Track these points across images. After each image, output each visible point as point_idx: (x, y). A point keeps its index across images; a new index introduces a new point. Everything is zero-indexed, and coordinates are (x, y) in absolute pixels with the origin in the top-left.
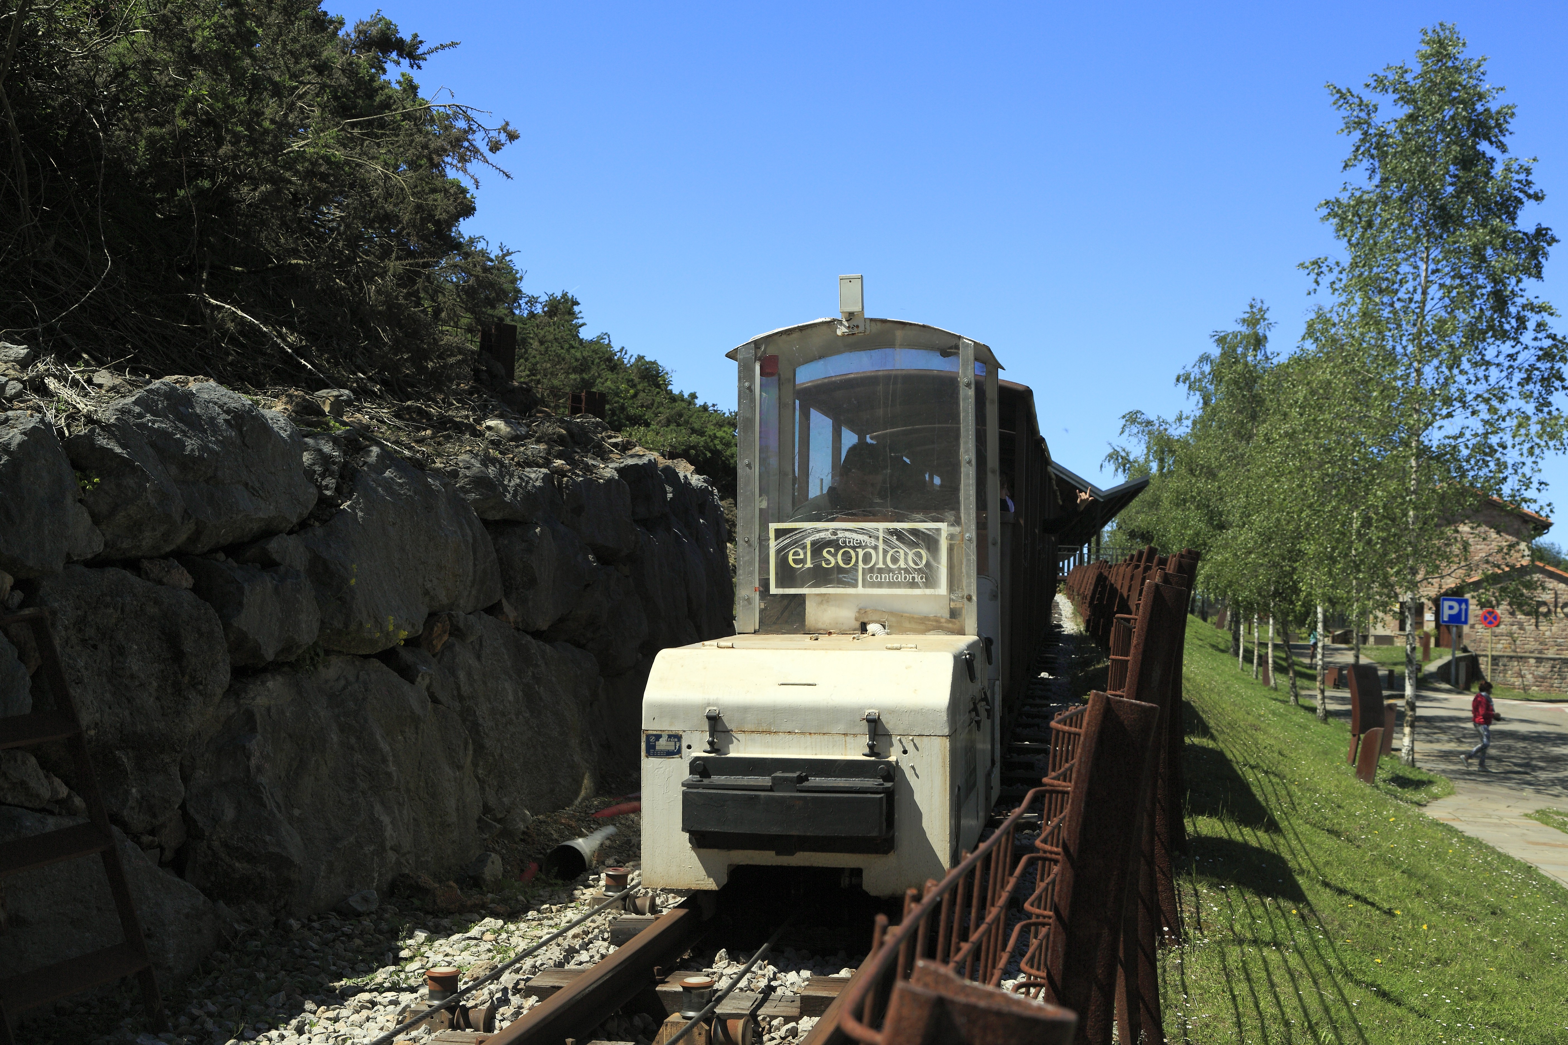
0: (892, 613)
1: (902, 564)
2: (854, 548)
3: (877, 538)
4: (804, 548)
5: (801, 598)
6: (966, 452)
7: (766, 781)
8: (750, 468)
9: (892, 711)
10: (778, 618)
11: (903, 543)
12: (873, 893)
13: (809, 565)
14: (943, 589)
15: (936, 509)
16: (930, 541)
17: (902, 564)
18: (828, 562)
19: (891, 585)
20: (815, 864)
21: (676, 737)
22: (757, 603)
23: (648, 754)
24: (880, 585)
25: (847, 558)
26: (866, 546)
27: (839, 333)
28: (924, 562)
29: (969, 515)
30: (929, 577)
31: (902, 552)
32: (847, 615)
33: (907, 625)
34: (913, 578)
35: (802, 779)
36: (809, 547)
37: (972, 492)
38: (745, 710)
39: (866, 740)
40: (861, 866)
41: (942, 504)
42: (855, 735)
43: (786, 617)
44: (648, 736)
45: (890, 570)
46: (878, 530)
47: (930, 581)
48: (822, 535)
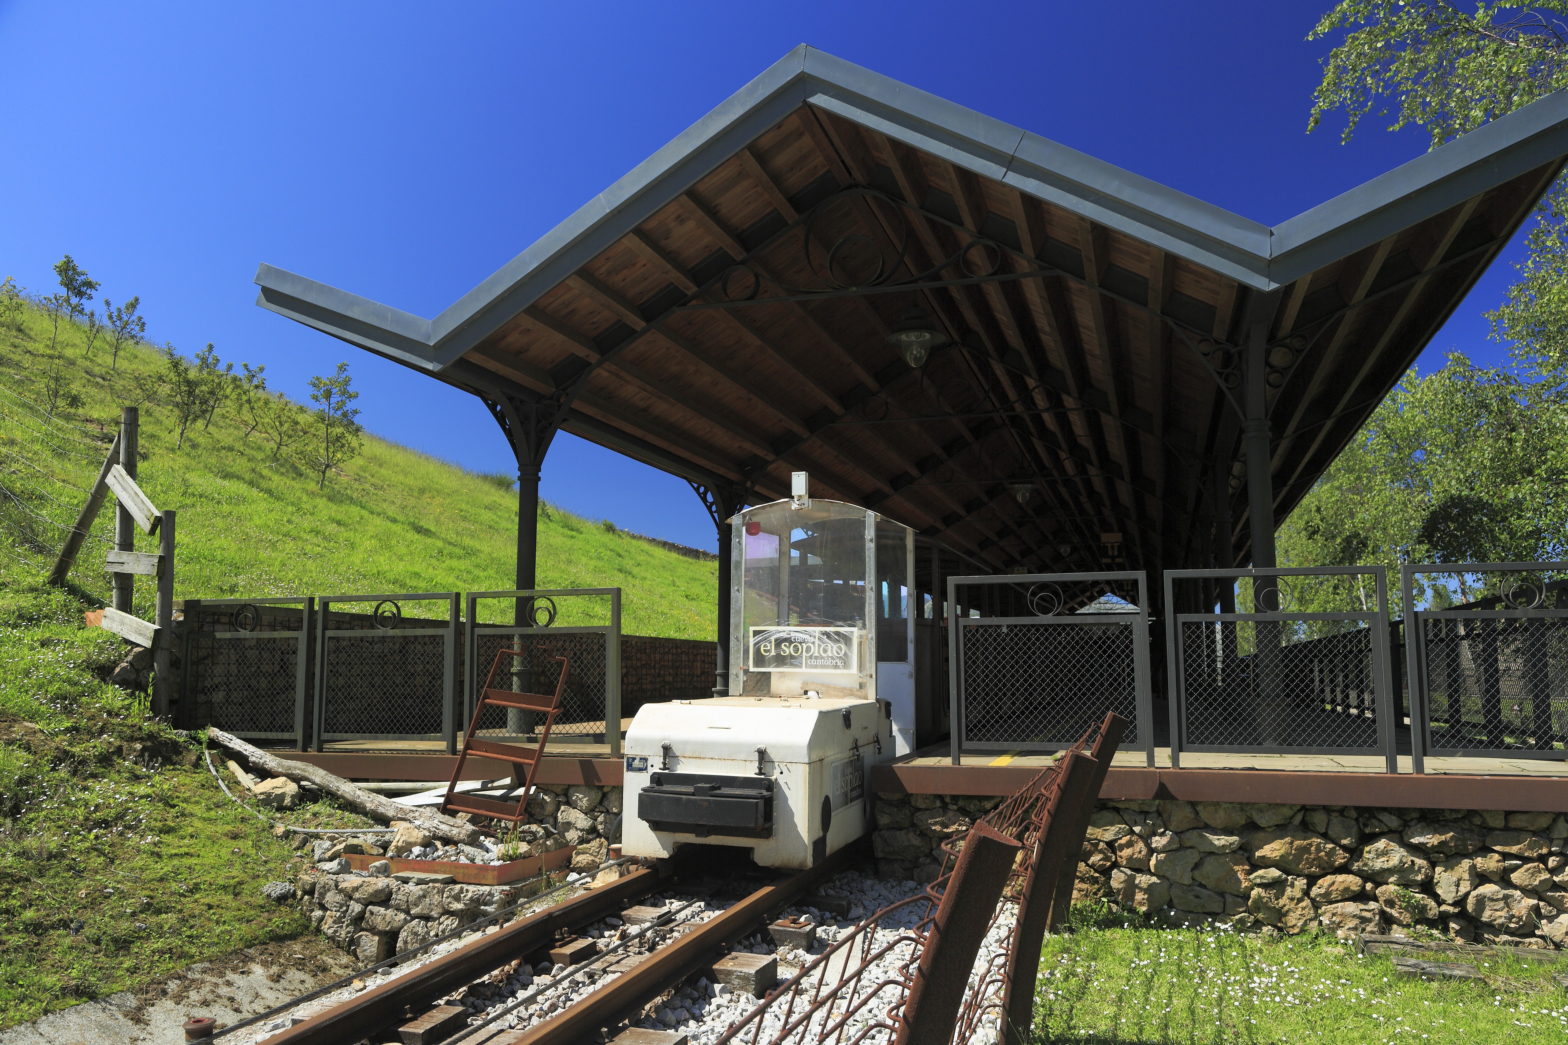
0: (823, 685)
7: (691, 789)
9: (773, 747)
12: (761, 864)
14: (854, 669)
18: (784, 651)
19: (823, 667)
21: (644, 760)
22: (742, 677)
23: (628, 770)
24: (816, 667)
25: (796, 649)
30: (845, 661)
32: (796, 685)
35: (714, 788)
38: (685, 743)
39: (757, 764)
43: (759, 686)
45: (822, 658)
47: (846, 664)
48: (781, 635)
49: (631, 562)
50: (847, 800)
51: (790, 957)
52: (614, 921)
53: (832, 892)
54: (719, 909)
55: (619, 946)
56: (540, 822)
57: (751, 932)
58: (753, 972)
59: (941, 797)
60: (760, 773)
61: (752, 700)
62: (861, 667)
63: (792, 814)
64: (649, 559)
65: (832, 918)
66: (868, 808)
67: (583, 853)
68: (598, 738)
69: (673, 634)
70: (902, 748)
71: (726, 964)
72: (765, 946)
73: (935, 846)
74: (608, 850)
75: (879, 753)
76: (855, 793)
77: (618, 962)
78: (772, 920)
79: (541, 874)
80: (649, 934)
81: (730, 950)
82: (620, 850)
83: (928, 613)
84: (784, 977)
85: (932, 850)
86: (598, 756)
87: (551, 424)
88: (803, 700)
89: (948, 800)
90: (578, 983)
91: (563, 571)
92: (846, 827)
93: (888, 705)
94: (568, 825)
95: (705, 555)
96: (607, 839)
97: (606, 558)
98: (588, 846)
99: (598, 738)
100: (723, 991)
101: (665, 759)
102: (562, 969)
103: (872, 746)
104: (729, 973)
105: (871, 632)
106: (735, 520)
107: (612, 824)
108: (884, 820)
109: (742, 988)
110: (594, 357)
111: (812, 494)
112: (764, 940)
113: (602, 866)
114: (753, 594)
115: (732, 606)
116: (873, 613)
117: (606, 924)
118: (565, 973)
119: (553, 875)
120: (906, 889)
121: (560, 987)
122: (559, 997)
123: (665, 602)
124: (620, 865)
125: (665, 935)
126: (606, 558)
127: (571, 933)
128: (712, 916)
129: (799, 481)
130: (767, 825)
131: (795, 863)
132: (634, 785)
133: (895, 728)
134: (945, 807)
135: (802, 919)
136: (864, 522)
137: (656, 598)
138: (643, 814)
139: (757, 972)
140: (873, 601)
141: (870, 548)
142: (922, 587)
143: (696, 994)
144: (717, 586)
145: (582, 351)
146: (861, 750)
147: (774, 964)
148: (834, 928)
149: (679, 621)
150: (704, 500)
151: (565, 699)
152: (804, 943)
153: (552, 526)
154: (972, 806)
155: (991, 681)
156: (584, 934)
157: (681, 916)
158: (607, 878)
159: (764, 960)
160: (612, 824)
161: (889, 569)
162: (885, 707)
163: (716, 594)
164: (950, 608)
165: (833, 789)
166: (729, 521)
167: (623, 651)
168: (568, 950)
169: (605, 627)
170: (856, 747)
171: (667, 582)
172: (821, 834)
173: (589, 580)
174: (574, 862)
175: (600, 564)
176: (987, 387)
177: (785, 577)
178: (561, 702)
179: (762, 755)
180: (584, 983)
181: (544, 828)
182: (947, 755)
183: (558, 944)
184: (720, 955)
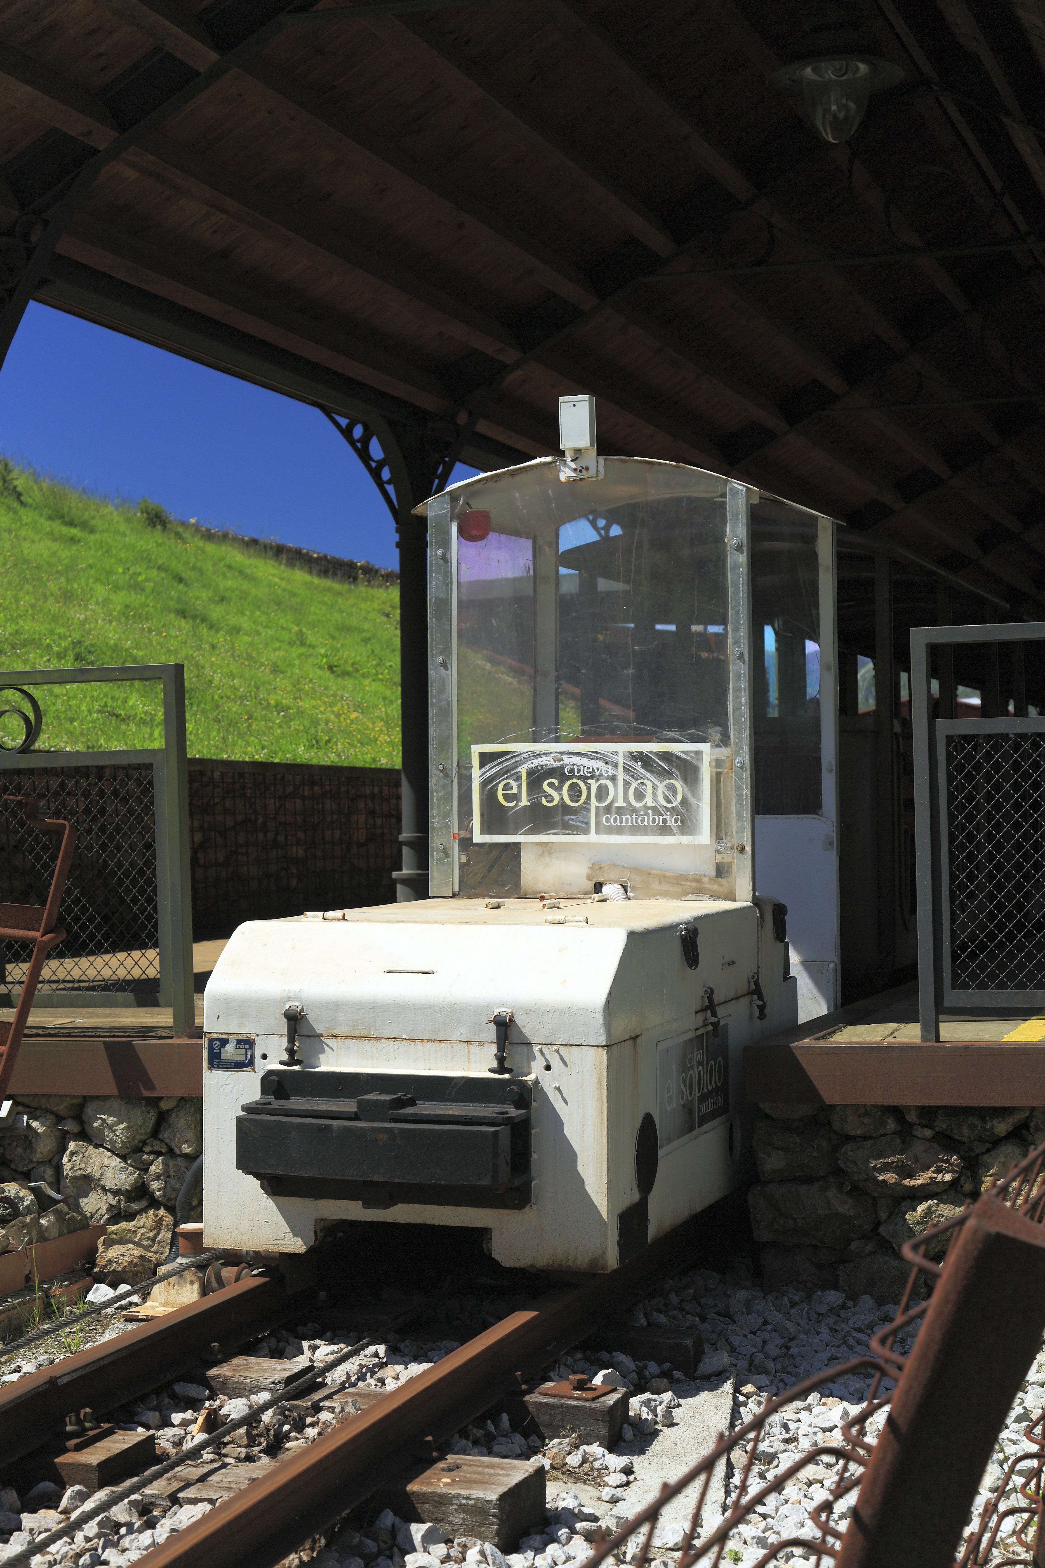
0: (636, 870)
1: (649, 801)
2: (584, 779)
3: (616, 765)
4: (518, 779)
5: (516, 848)
6: (736, 643)
7: (349, 1106)
8: (446, 668)
9: (529, 1011)
10: (484, 877)
11: (651, 772)
12: (506, 1262)
13: (524, 802)
14: (704, 835)
15: (696, 724)
16: (687, 770)
17: (649, 801)
18: (550, 798)
19: (635, 830)
20: (429, 1222)
21: (247, 1043)
22: (457, 856)
23: (212, 1066)
24: (619, 830)
26: (601, 776)
27: (563, 477)
28: (679, 798)
29: (740, 732)
30: (685, 819)
31: (649, 784)
32: (573, 871)
33: (656, 886)
34: (665, 821)
35: (399, 1103)
36: (524, 777)
37: (745, 699)
38: (336, 1006)
39: (493, 1049)
40: (490, 1225)
41: (706, 718)
42: (481, 1043)
43: (495, 877)
44: (211, 1041)
45: (634, 810)
46: (616, 753)
47: (687, 825)
48: (542, 761)
49: (204, 594)
50: (692, 1121)
51: (573, 1460)
52: (192, 1390)
53: (662, 1318)
54: (418, 1358)
55: (203, 1446)
56: (24, 1177)
57: (487, 1410)
58: (493, 1497)
59: (897, 1112)
60: (501, 1069)
61: (478, 906)
62: (719, 829)
63: (572, 1156)
64: (246, 585)
65: (664, 1374)
66: (738, 1135)
67: (120, 1242)
68: (145, 992)
69: (302, 753)
70: (811, 1003)
71: (436, 1482)
72: (518, 1438)
73: (883, 1216)
74: (175, 1235)
75: (762, 1016)
76: (709, 1106)
77: (202, 1479)
78: (534, 1383)
79: (30, 1289)
80: (267, 1417)
81: (444, 1450)
82: (199, 1234)
83: (866, 701)
84: (562, 1504)
85: (878, 1224)
86: (145, 1032)
87: (11, 292)
88: (591, 907)
89: (912, 1117)
90: (118, 1525)
91: (55, 618)
92: (691, 1177)
93: (780, 911)
94: (87, 1183)
95: (370, 572)
96: (171, 1210)
97: (149, 585)
98: (131, 1225)
99: (145, 992)
100: (429, 1538)
101: (291, 1040)
102: (83, 1497)
103: (744, 1001)
104: (442, 1500)
105: (740, 753)
106: (433, 508)
107: (180, 1179)
108: (773, 1162)
109: (473, 1531)
110: (103, 137)
111: (607, 442)
112: (516, 1426)
113: (162, 1270)
114: (479, 660)
115: (432, 700)
116: (745, 709)
117: (174, 1396)
118: (89, 1505)
119: (57, 1290)
120: (823, 1309)
121: (79, 1536)
122: (79, 1555)
123: (281, 682)
124: (201, 1267)
125: (302, 1419)
126: (149, 585)
127: (98, 1420)
128: (404, 1376)
129: (576, 418)
130: (517, 1182)
131: (581, 1259)
132: (226, 1098)
133: (794, 958)
134: (905, 1132)
135: (598, 1380)
136: (723, 506)
137: (263, 674)
138: (247, 1161)
139: (503, 1497)
140: (744, 684)
141: (737, 564)
142: (851, 643)
143: (372, 1546)
144: (397, 642)
145: (75, 123)
146: (721, 1011)
147: (539, 1477)
148: (667, 1396)
149: (315, 723)
150: (364, 455)
151: (69, 910)
152: (604, 1431)
153: (26, 515)
154: (966, 1131)
155: (1008, 857)
156: (128, 1421)
157: (338, 1375)
158: (172, 1299)
159: (518, 1471)
160: (180, 1179)
161: (779, 599)
162: (773, 917)
163: (395, 661)
164: (917, 686)
165: (662, 1099)
166: (419, 509)
167: (193, 795)
168: (94, 1456)
169: (153, 752)
170: (710, 1006)
171: (286, 636)
172: (636, 1197)
173: (111, 635)
174: (100, 1261)
175: (136, 599)
176: (998, 185)
177: (548, 622)
178: (61, 919)
179: (505, 1029)
180: (129, 1526)
181: (33, 1190)
182: (909, 1017)
183: (72, 1443)
184: (423, 1462)
